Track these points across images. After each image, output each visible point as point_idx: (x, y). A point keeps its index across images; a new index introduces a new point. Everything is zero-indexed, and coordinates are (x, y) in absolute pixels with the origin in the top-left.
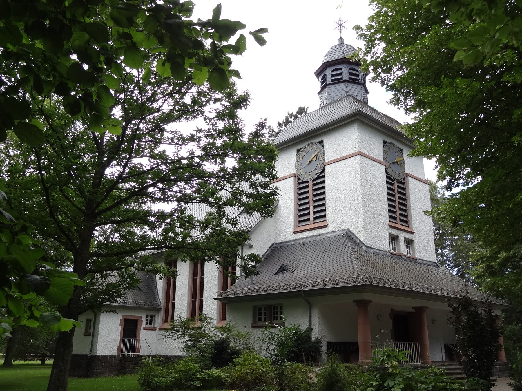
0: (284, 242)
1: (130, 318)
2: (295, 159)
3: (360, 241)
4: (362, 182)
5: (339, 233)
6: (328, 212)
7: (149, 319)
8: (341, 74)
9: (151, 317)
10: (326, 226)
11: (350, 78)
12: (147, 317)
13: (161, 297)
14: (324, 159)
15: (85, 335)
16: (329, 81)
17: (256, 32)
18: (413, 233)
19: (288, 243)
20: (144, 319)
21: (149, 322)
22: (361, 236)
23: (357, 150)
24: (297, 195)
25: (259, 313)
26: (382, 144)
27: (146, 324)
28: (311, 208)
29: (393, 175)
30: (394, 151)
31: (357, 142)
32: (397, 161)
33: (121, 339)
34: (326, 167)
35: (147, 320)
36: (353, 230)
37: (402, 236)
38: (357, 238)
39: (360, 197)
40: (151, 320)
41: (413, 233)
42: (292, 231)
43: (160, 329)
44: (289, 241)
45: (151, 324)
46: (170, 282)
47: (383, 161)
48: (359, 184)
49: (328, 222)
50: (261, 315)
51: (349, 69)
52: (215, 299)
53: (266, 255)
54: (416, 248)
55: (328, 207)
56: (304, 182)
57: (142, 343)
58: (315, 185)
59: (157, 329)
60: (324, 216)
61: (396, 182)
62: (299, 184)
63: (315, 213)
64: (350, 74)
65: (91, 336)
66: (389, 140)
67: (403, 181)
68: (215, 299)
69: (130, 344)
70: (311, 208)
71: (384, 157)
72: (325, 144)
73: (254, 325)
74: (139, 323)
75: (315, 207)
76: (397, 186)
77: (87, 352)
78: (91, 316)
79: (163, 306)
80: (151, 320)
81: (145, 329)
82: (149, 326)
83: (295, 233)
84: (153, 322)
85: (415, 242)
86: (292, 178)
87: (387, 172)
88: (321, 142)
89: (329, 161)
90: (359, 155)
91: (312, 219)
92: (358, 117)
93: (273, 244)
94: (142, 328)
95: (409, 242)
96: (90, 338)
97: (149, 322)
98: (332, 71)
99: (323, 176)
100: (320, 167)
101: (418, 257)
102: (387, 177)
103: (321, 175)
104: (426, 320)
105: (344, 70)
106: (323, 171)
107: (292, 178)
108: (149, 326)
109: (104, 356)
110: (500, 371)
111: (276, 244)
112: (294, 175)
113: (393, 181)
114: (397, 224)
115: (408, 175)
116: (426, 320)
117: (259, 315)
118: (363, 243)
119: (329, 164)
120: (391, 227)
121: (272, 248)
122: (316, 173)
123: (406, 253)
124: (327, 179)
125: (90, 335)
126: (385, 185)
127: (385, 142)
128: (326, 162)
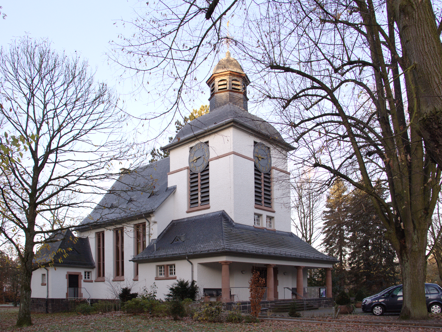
0: (180, 219)
1: (73, 274)
2: (189, 155)
3: (231, 219)
4: (234, 175)
5: (218, 213)
6: (211, 198)
7: (87, 274)
9: (89, 273)
10: (209, 208)
12: (85, 273)
13: (94, 261)
14: (209, 156)
15: (42, 285)
18: (274, 212)
19: (183, 220)
20: (83, 274)
21: (87, 276)
22: (232, 215)
23: (232, 151)
24: (190, 184)
25: (160, 270)
27: (85, 278)
28: (199, 194)
29: (260, 168)
31: (232, 144)
33: (68, 288)
34: (210, 162)
35: (85, 275)
36: (228, 212)
37: (265, 214)
38: (229, 217)
39: (232, 187)
40: (88, 275)
41: (274, 212)
42: (186, 211)
43: (95, 281)
44: (184, 219)
45: (88, 278)
46: (100, 248)
47: (253, 158)
48: (232, 177)
49: (210, 204)
50: (162, 271)
52: (130, 261)
53: (167, 229)
54: (276, 223)
55: (211, 193)
56: (194, 174)
57: (83, 291)
58: (202, 176)
59: (94, 282)
60: (208, 200)
61: (262, 174)
62: (191, 175)
63: (202, 197)
65: (46, 286)
66: (258, 141)
67: (269, 173)
68: (130, 261)
69: (74, 291)
70: (199, 194)
72: (210, 144)
73: (156, 279)
74: (79, 278)
75: (202, 193)
77: (45, 297)
78: (44, 271)
79: (96, 265)
80: (88, 275)
81: (85, 281)
82: (87, 279)
83: (188, 212)
84: (90, 277)
85: (275, 218)
86: (186, 170)
87: (255, 166)
88: (207, 142)
89: (212, 158)
91: (200, 202)
92: (232, 124)
93: (173, 221)
94: (82, 281)
95: (270, 218)
96: (46, 287)
97: (87, 276)
99: (208, 170)
100: (205, 162)
101: (277, 230)
103: (206, 169)
106: (208, 165)
107: (186, 170)
108: (87, 279)
109: (278, 295)
110: (326, 304)
111: (175, 221)
112: (188, 168)
113: (260, 172)
114: (262, 205)
117: (160, 272)
118: (233, 221)
119: (212, 160)
120: (256, 208)
121: (172, 223)
122: (202, 168)
123: (268, 227)
124: (211, 172)
125: (45, 285)
126: (253, 176)
128: (210, 158)
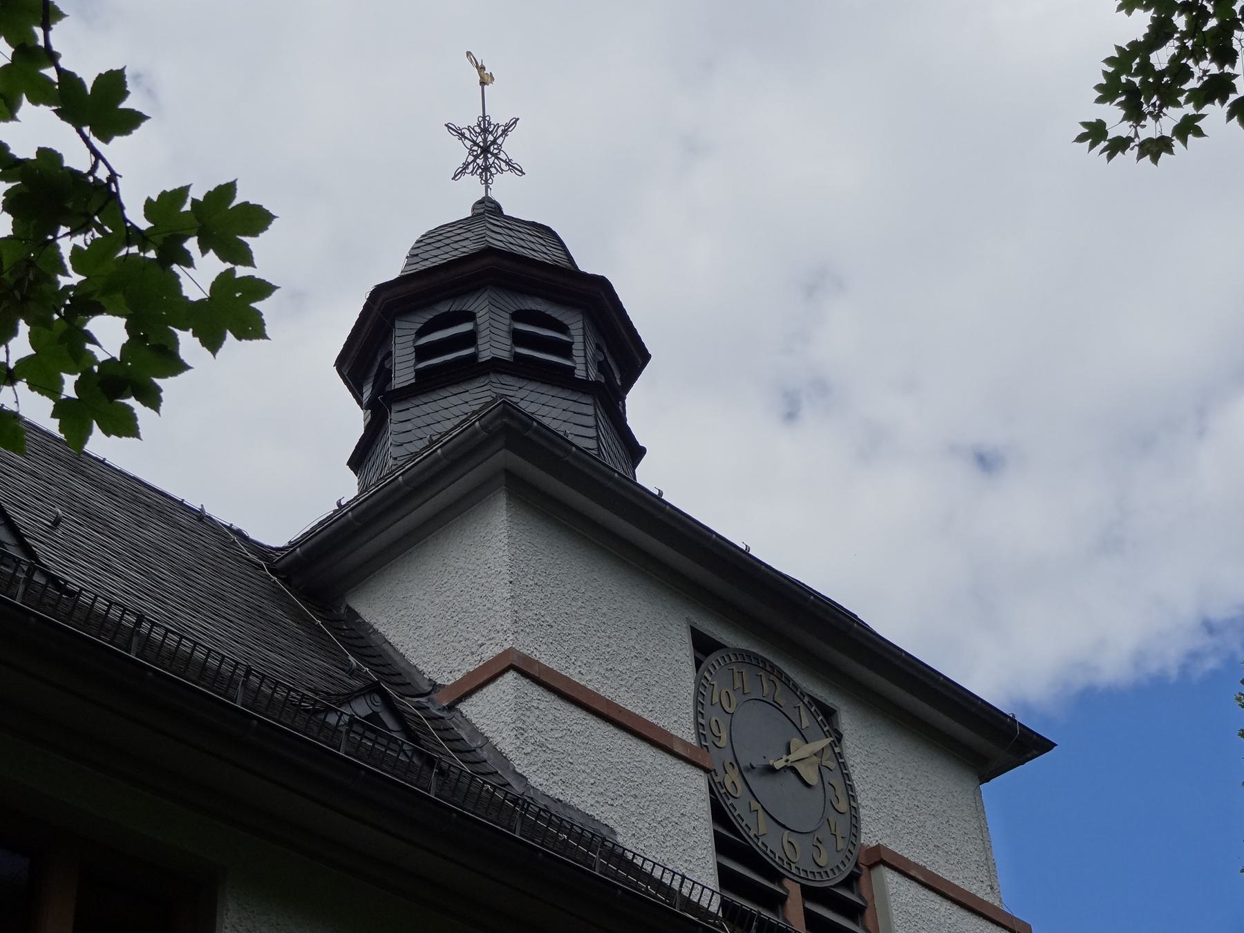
8: (470, 339)
11: (517, 356)
16: (403, 375)
17: (104, 301)
26: (684, 653)
29: (772, 842)
30: (778, 707)
32: (792, 757)
51: (518, 316)
61: (794, 891)
64: (518, 338)
71: (698, 725)
76: (808, 914)
90: (510, 676)
98: (421, 333)
102: (723, 846)
104: (633, 348)
105: (483, 316)
113: (777, 877)
115: (879, 858)
116: (633, 348)
127: (703, 646)
